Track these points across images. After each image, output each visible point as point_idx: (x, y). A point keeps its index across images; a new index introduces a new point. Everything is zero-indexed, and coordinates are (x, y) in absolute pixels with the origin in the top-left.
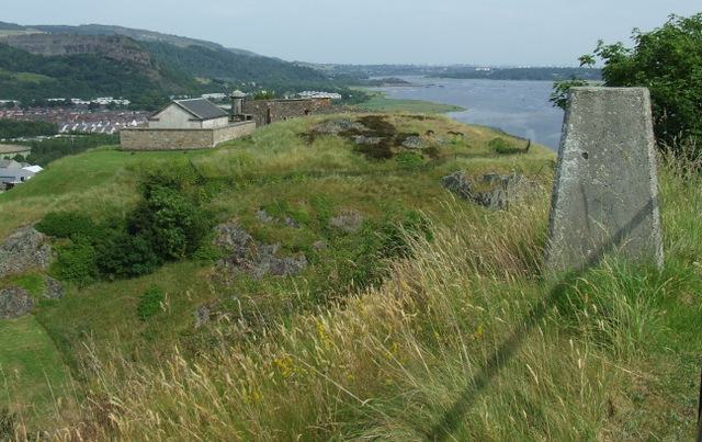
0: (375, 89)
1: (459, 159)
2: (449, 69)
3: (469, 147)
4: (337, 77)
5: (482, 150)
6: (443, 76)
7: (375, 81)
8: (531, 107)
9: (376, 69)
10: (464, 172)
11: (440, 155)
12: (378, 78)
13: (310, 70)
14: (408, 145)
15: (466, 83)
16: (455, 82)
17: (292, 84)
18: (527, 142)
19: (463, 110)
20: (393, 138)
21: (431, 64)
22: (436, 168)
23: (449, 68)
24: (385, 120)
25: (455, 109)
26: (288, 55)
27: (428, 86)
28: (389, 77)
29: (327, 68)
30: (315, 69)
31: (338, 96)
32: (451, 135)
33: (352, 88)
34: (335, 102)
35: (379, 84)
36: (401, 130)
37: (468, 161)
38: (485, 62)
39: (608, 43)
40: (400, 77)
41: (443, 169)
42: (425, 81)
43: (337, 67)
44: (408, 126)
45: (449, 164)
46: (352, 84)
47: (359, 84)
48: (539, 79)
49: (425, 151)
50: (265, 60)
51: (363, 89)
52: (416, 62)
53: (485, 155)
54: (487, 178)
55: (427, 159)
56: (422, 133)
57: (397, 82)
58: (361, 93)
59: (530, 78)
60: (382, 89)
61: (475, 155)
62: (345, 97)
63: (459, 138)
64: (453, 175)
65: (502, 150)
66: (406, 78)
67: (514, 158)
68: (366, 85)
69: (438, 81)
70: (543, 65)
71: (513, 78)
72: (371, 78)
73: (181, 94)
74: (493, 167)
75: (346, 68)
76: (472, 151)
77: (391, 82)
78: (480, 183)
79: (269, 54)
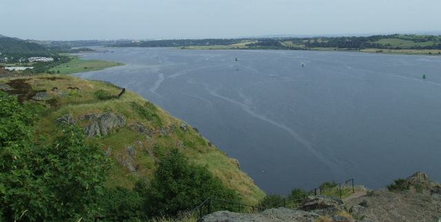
0: (75, 54)
1: (70, 106)
2: (118, 41)
3: (81, 96)
4: (52, 48)
5: (90, 97)
7: (75, 50)
10: (71, 115)
13: (36, 45)
14: (37, 98)
15: (126, 49)
16: (119, 49)
17: (25, 53)
18: (121, 91)
20: (27, 94)
21: (108, 40)
22: (53, 112)
24: (27, 82)
26: (23, 36)
27: (105, 52)
29: (47, 43)
30: (40, 44)
31: (51, 59)
32: (70, 90)
33: (61, 54)
36: (35, 88)
37: (75, 107)
38: (137, 37)
39: (389, 185)
40: (90, 47)
41: (57, 114)
42: (103, 49)
44: (43, 85)
45: (61, 110)
48: (166, 46)
49: (48, 102)
50: (8, 39)
51: (68, 54)
52: (99, 38)
53: (89, 102)
54: (87, 117)
55: (49, 106)
57: (88, 50)
58: (65, 57)
59: (161, 46)
60: (79, 54)
61: (82, 103)
62: (56, 59)
63: (75, 91)
64: (63, 117)
65: (101, 97)
66: (92, 48)
69: (110, 49)
70: (168, 39)
71: (152, 46)
72: (73, 48)
73: (23, 55)
74: (91, 109)
76: (81, 100)
78: (82, 121)
79: (12, 35)
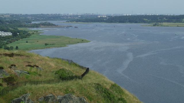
0: (35, 29)
1: (28, 85)
2: (82, 16)
3: (40, 75)
5: (51, 77)
6: (77, 21)
7: (36, 24)
8: (129, 39)
9: (37, 17)
11: (15, 83)
12: (37, 23)
15: (91, 25)
19: (87, 42)
23: (81, 16)
25: (83, 41)
27: (68, 27)
28: (44, 22)
29: (6, 16)
31: (10, 34)
32: (29, 67)
33: (20, 29)
34: (7, 38)
35: (37, 26)
37: (33, 86)
43: (12, 16)
45: (19, 89)
46: (21, 26)
47: (25, 26)
48: (136, 22)
52: (62, 13)
55: (5, 85)
56: (6, 67)
58: (25, 32)
60: (40, 29)
61: (41, 82)
62: (15, 34)
63: (34, 69)
64: (21, 98)
67: (69, 83)
68: (29, 27)
69: (74, 24)
70: (139, 14)
72: (33, 23)
75: (17, 16)
76: (40, 79)
77: (44, 25)
